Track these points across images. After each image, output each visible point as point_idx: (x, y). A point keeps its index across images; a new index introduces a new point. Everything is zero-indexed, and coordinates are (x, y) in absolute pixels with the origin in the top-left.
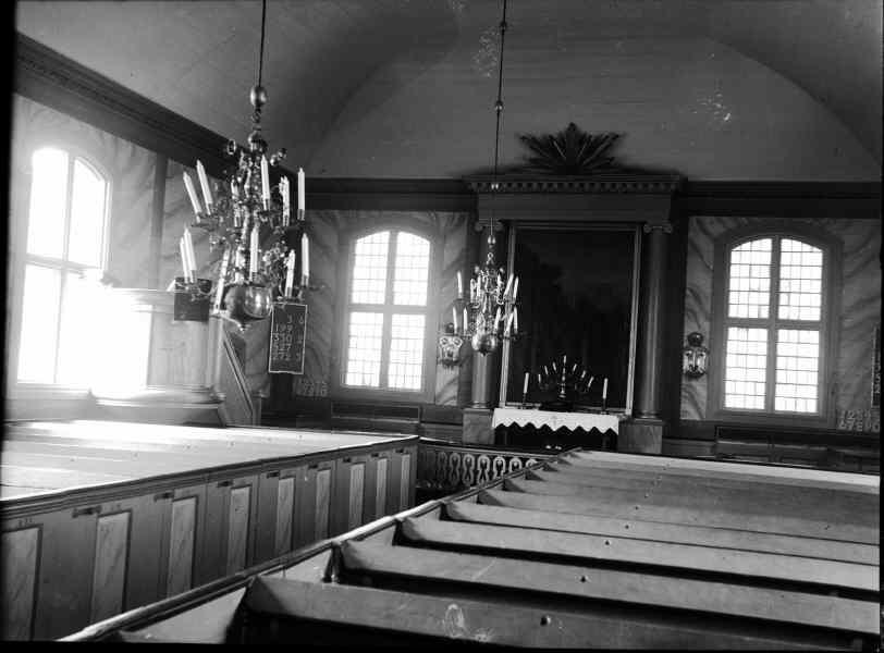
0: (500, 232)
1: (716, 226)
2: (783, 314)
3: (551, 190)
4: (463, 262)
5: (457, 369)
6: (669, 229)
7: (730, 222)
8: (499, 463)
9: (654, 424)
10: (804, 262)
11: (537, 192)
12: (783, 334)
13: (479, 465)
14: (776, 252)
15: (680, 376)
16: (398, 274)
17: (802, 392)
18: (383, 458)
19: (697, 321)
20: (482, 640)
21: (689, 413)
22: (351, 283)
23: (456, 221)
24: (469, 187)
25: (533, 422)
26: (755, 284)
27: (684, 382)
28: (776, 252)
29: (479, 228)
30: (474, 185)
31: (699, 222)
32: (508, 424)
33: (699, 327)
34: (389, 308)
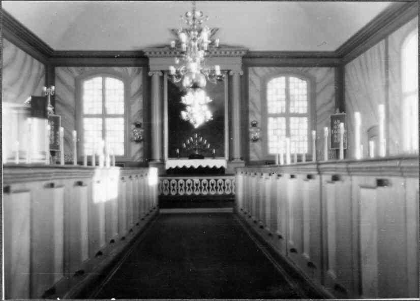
0: (241, 77)
1: (261, 71)
2: (292, 110)
3: (156, 55)
4: (142, 92)
5: (142, 143)
6: (242, 73)
7: (266, 69)
8: (166, 183)
9: (241, 163)
10: (299, 87)
11: (224, 56)
12: (292, 119)
13: (218, 184)
14: (287, 83)
15: (249, 141)
16: (108, 98)
17: (301, 145)
18: (60, 186)
19: (254, 115)
20: (59, 280)
21: (253, 157)
22: (307, 98)
23: (137, 71)
24: (145, 55)
25: (186, 165)
26: (279, 97)
27: (251, 143)
28: (287, 83)
29: (150, 74)
30: (147, 54)
31: (253, 70)
32: (174, 167)
33: (256, 118)
34: (104, 115)
